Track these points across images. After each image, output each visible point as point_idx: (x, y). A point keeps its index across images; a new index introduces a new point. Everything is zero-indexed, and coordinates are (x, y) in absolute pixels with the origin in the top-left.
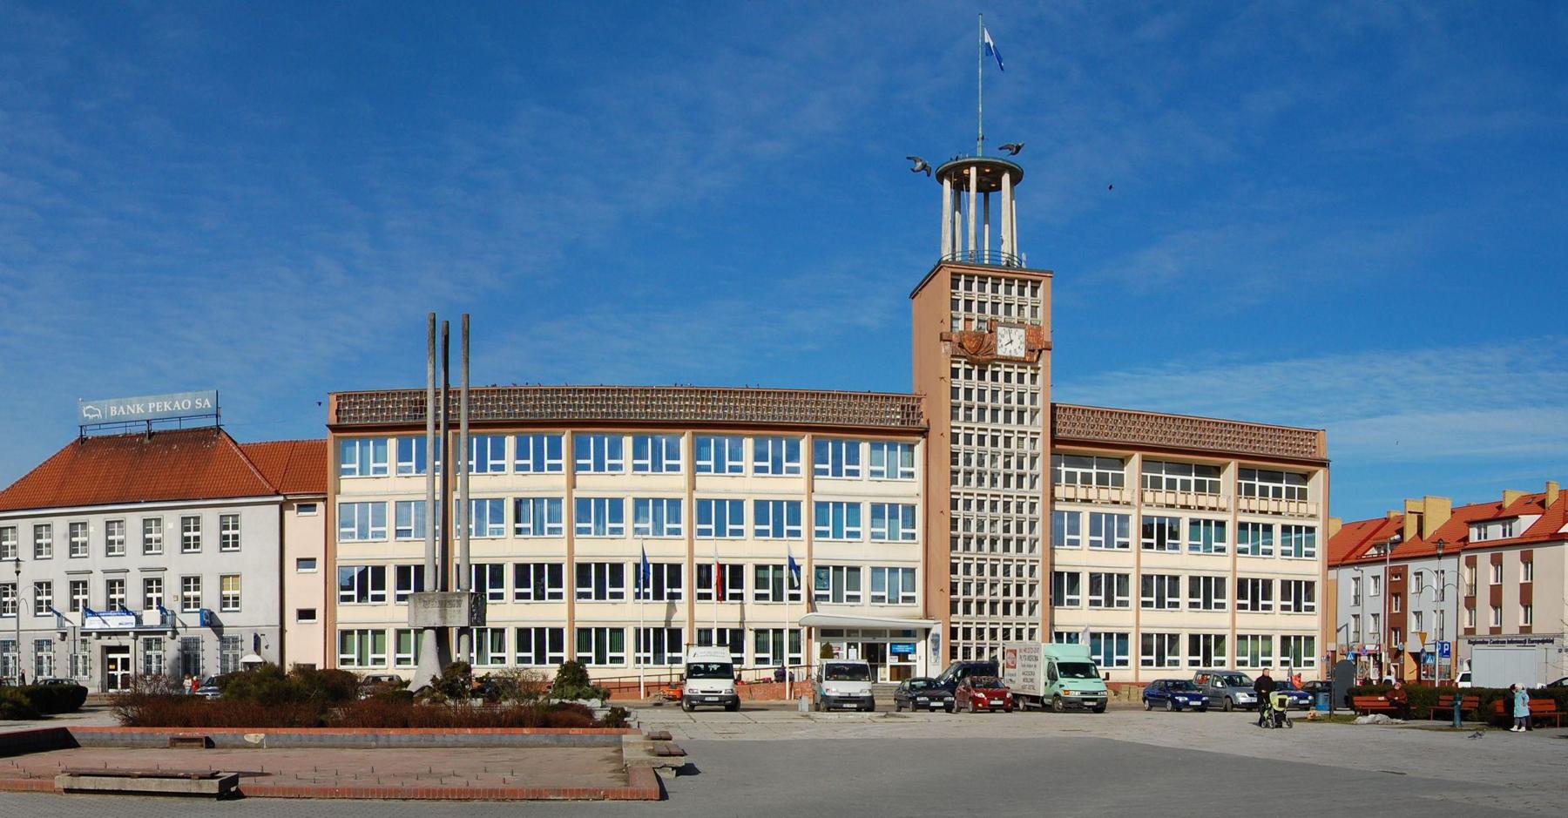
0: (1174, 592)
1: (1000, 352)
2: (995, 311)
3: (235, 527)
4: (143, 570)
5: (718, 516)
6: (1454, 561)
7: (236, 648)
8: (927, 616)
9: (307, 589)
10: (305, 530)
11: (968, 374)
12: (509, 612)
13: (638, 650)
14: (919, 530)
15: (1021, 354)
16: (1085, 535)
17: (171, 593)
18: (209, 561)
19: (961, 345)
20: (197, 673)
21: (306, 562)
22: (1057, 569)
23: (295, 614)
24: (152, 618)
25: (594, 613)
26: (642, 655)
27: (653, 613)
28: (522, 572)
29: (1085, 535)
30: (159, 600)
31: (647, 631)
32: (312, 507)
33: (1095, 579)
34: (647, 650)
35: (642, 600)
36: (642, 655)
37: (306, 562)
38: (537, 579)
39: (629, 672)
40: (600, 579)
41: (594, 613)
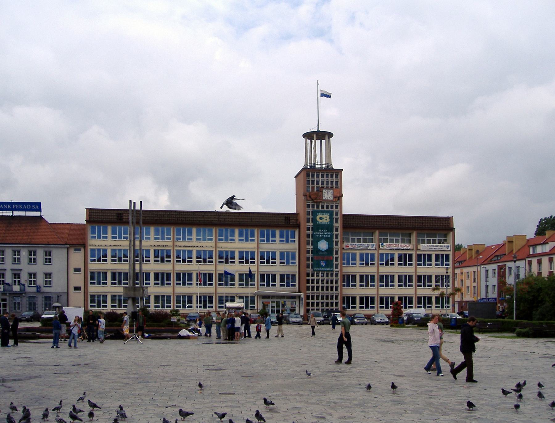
0: (393, 281)
1: (324, 198)
2: (322, 184)
3: (50, 255)
4: (12, 270)
5: (226, 257)
6: (524, 261)
7: (50, 300)
8: (299, 292)
9: (77, 279)
10: (77, 258)
11: (313, 206)
12: (153, 289)
13: (197, 304)
14: (297, 261)
15: (332, 199)
16: (358, 261)
17: (24, 278)
18: (40, 268)
19: (310, 197)
20: (35, 309)
21: (77, 270)
22: (344, 274)
23: (73, 270)
24: (16, 288)
25: (182, 290)
26: (199, 305)
27: (245, 268)
28: (157, 275)
29: (358, 261)
30: (19, 281)
31: (200, 297)
32: (79, 250)
33: (362, 277)
34: (200, 303)
35: (199, 286)
36: (199, 305)
37: (77, 270)
38: (162, 278)
39: (194, 311)
40: (184, 278)
41: (182, 290)
